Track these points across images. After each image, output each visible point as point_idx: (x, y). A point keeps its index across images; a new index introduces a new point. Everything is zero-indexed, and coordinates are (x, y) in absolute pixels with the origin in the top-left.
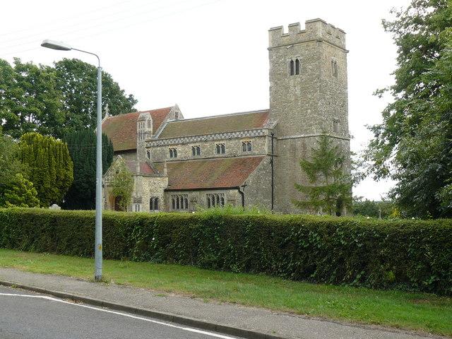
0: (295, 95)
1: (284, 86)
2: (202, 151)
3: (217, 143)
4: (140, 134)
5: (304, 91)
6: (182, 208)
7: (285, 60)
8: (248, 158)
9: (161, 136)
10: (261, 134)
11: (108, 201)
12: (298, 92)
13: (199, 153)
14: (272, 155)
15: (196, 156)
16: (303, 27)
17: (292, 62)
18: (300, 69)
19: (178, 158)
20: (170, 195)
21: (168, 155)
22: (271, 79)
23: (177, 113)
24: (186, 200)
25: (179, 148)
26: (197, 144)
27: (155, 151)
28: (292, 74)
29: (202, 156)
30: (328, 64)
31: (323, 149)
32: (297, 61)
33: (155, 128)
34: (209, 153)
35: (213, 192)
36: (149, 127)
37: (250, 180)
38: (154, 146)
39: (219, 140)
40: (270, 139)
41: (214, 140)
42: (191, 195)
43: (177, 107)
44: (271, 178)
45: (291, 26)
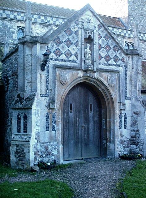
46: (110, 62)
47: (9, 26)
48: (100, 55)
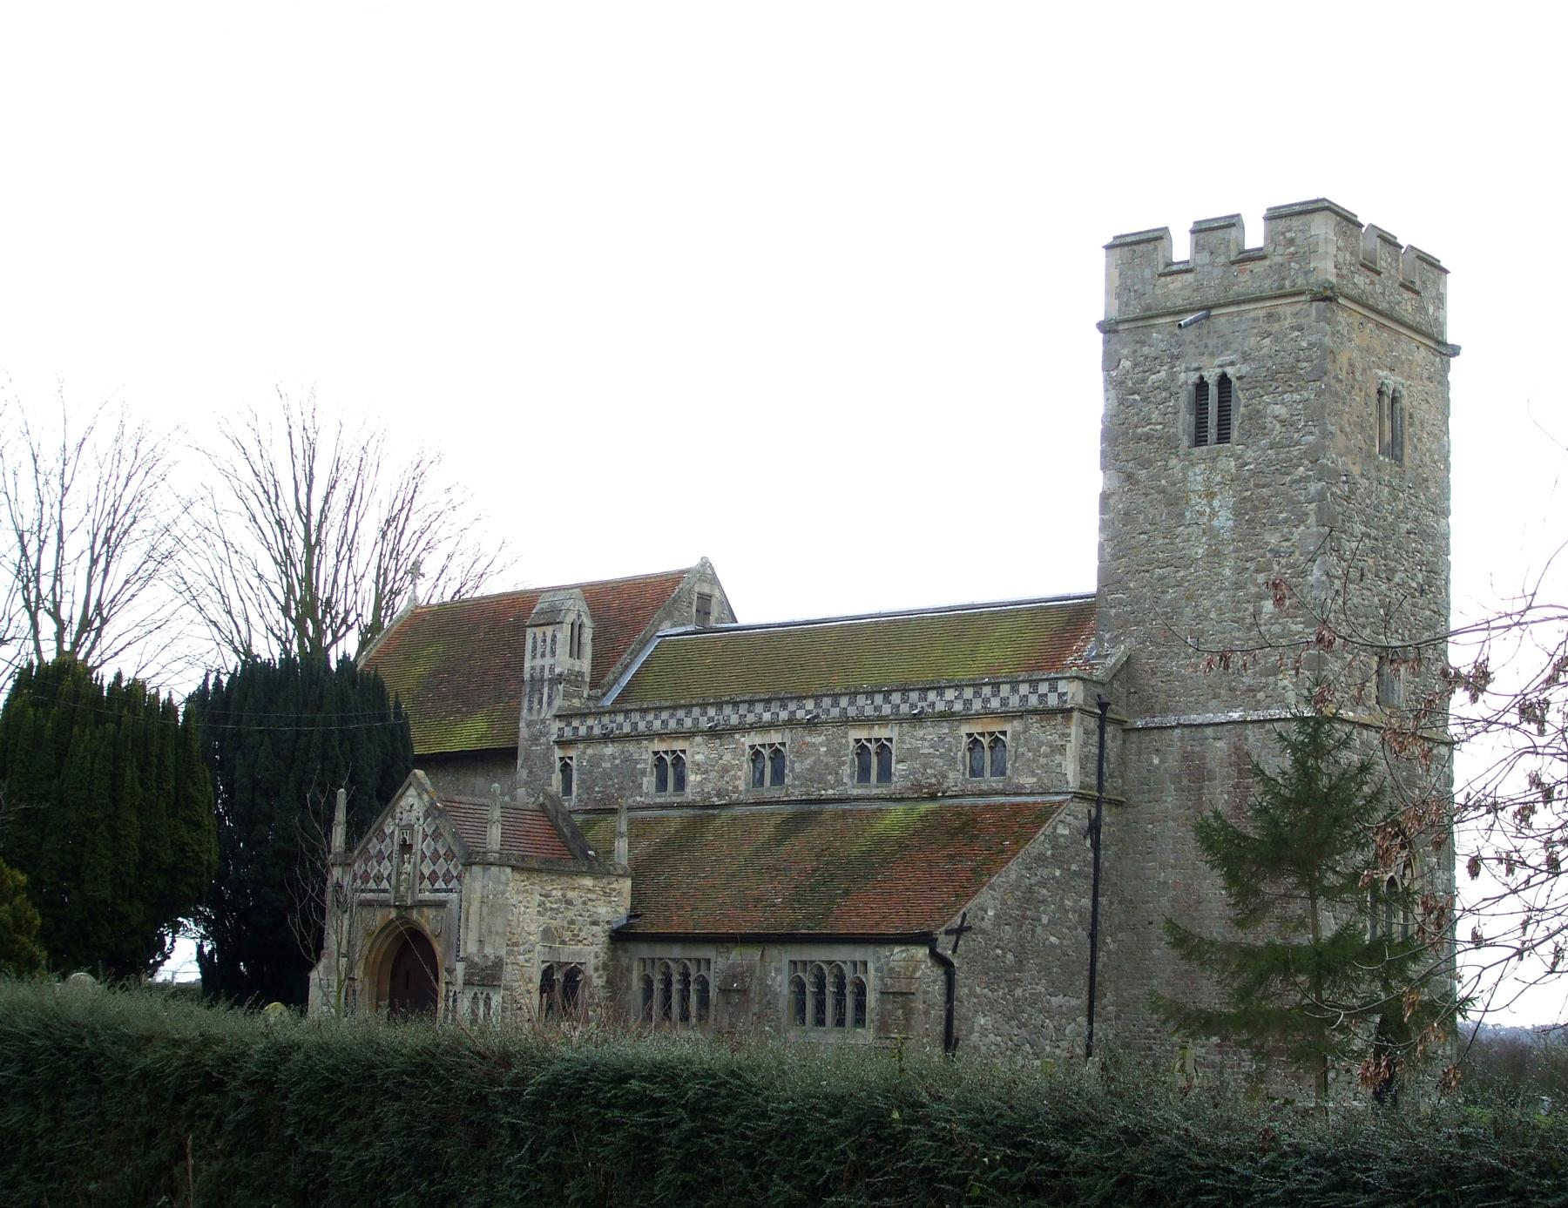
0: (1211, 532)
1: (1162, 491)
2: (796, 767)
3: (862, 734)
4: (536, 682)
5: (1249, 513)
6: (685, 1017)
7: (1173, 376)
8: (990, 808)
9: (623, 697)
10: (1053, 700)
11: (358, 973)
12: (1224, 520)
13: (778, 776)
14: (1097, 796)
15: (769, 791)
16: (1254, 237)
17: (1202, 386)
18: (1236, 421)
19: (690, 794)
20: (636, 959)
21: (649, 782)
22: (1110, 460)
23: (705, 599)
24: (704, 983)
25: (697, 752)
26: (775, 738)
27: (596, 761)
28: (1199, 439)
29: (794, 787)
30: (1361, 403)
31: (1306, 774)
32: (1224, 381)
33: (601, 664)
34: (821, 779)
35: (819, 954)
36: (576, 650)
37: (987, 905)
38: (589, 740)
39: (868, 722)
40: (1092, 724)
41: (846, 721)
42: (721, 962)
43: (705, 573)
44: (1086, 902)
45: (1202, 230)
46: (437, 886)
47: (636, 756)
48: (422, 873)
